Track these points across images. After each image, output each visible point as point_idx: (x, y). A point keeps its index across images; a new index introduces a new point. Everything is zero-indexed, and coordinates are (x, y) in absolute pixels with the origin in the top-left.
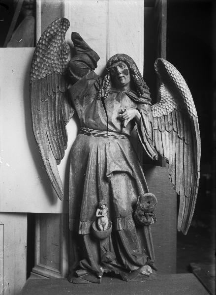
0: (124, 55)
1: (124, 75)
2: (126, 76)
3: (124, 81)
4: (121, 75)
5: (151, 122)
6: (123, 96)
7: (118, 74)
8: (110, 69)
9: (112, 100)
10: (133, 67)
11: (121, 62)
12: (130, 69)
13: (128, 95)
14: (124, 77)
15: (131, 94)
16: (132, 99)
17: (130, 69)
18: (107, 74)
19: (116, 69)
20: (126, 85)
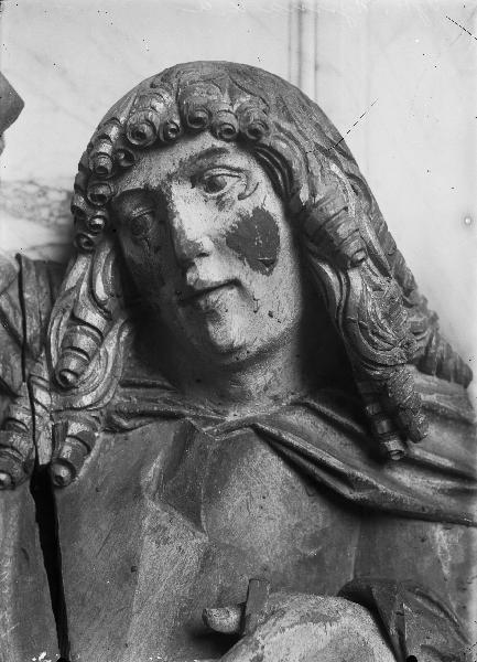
0: (241, 77)
1: (239, 270)
2: (256, 283)
3: (236, 327)
4: (210, 270)
5: (24, 551)
6: (228, 457)
7: (181, 259)
8: (110, 204)
9: (129, 492)
10: (326, 190)
11: (207, 141)
12: (298, 215)
13: (276, 445)
14: (234, 283)
15: (309, 430)
16: (312, 476)
17: (298, 215)
18: (91, 250)
19: (157, 201)
20: (263, 356)
